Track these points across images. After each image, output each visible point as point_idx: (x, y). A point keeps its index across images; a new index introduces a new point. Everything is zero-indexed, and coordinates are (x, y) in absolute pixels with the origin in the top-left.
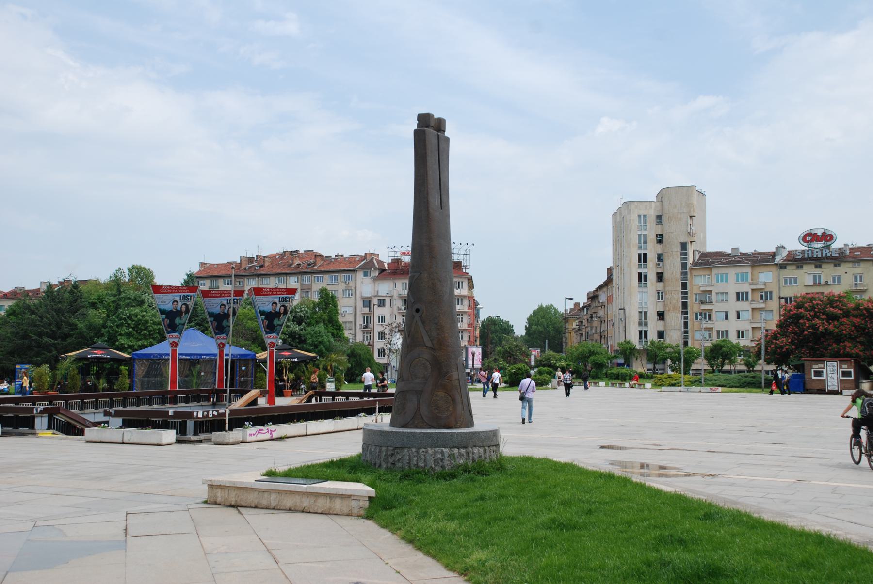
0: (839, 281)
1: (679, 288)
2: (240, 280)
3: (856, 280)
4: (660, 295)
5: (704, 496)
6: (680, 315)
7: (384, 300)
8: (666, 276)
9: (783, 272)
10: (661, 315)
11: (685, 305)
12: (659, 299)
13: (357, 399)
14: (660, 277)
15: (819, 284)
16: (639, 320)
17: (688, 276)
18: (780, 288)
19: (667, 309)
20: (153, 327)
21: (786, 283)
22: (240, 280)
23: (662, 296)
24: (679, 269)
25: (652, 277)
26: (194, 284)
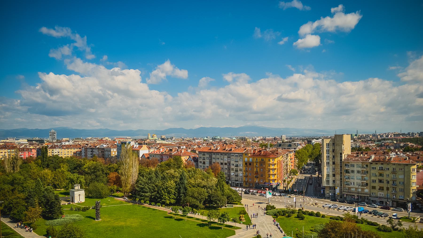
0: (388, 169)
1: (339, 167)
2: (393, 199)
3: (394, 169)
4: (334, 169)
5: (66, 77)
6: (339, 176)
7: (251, 163)
8: (335, 163)
9: (371, 165)
10: (334, 175)
11: (341, 173)
12: (387, 176)
13: (281, 229)
14: (334, 163)
15: (383, 169)
16: (145, 145)
17: (342, 164)
18: (370, 170)
19: (336, 174)
20: (153, 195)
21: (372, 169)
22: (393, 199)
23: (334, 169)
24: (339, 161)
25: (331, 163)
26: (27, 204)
